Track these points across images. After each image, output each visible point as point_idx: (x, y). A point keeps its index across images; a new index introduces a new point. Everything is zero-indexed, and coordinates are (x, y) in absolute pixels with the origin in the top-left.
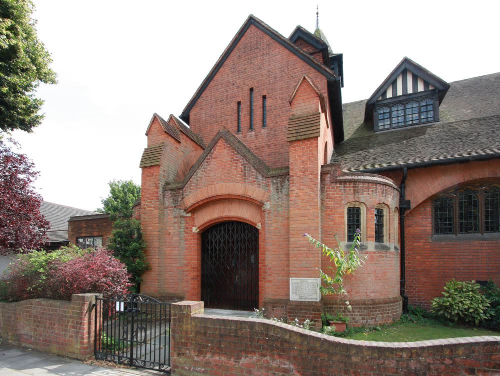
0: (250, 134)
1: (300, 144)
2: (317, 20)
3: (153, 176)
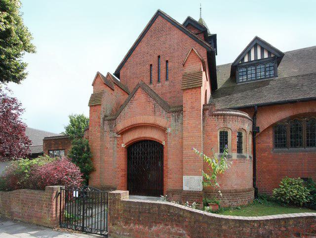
1: (189, 91)
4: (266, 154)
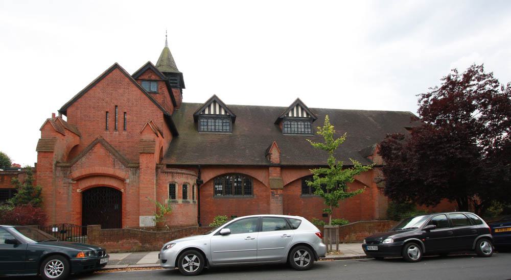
1: (145, 154)
4: (209, 199)
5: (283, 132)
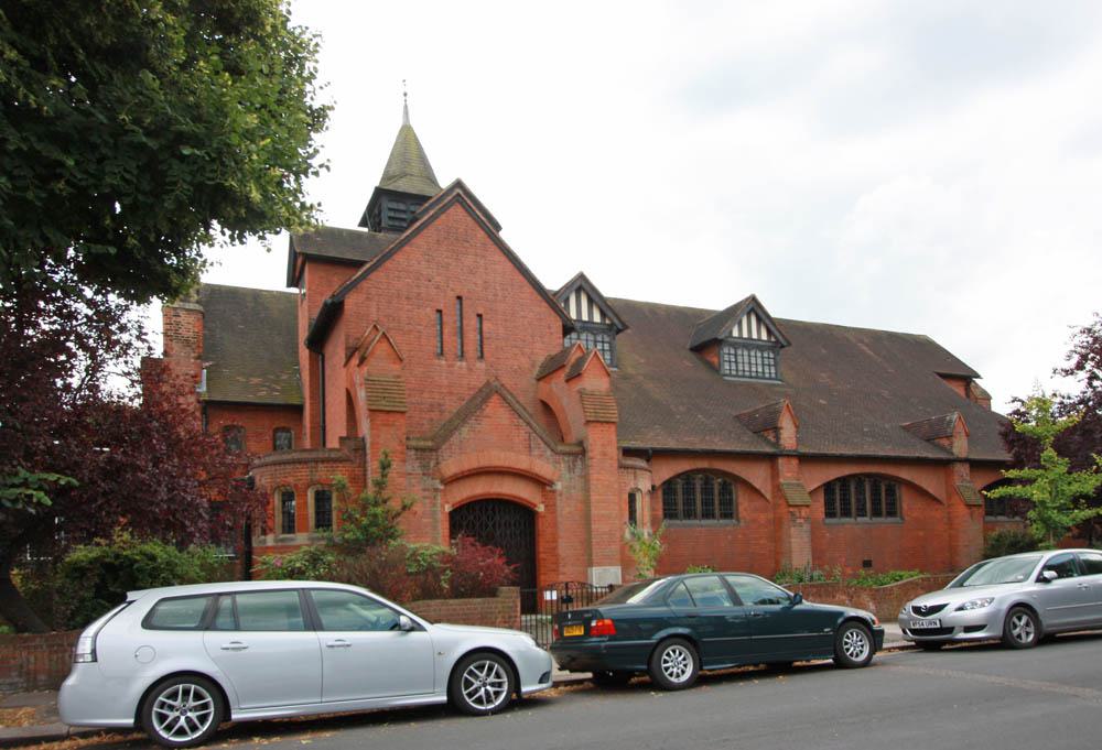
0: (459, 363)
1: (599, 425)
2: (406, 107)
3: (393, 425)
5: (722, 372)
